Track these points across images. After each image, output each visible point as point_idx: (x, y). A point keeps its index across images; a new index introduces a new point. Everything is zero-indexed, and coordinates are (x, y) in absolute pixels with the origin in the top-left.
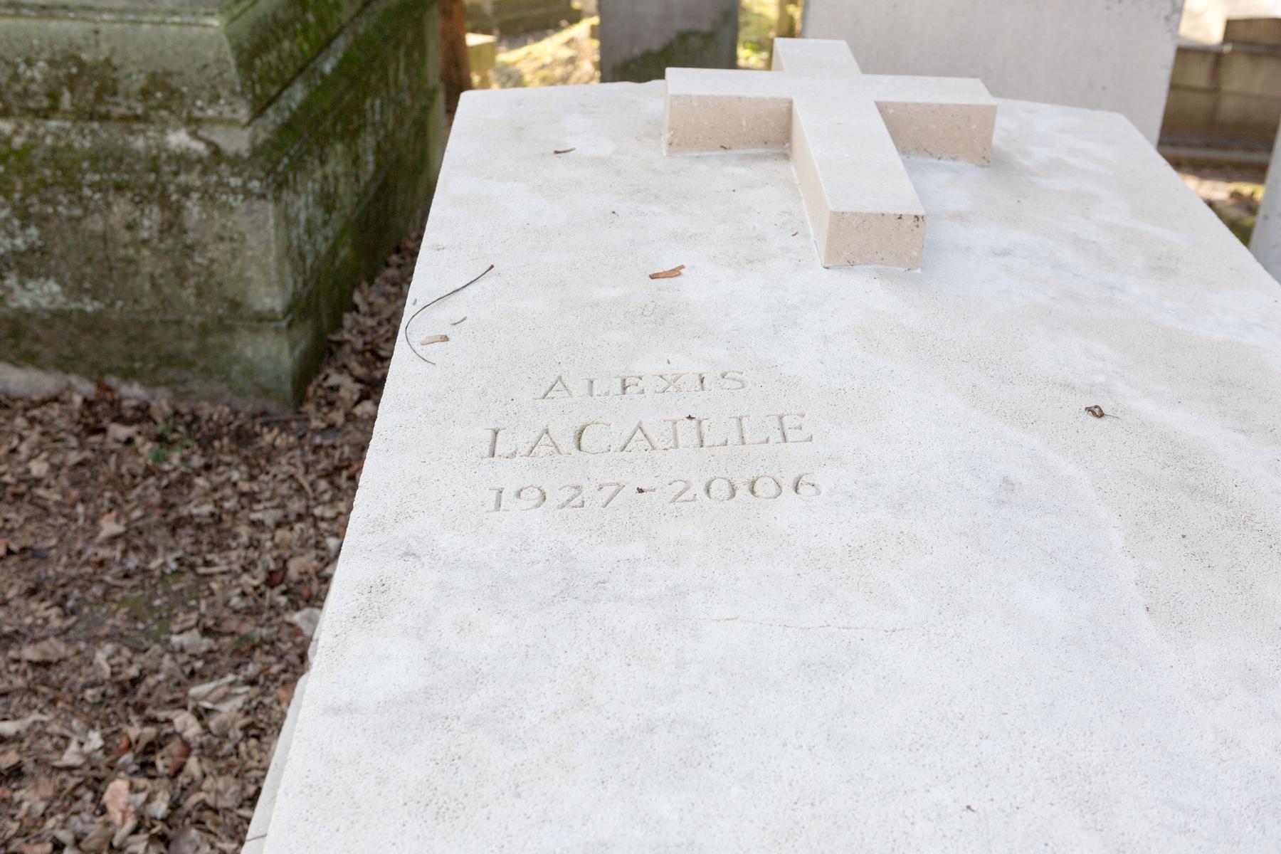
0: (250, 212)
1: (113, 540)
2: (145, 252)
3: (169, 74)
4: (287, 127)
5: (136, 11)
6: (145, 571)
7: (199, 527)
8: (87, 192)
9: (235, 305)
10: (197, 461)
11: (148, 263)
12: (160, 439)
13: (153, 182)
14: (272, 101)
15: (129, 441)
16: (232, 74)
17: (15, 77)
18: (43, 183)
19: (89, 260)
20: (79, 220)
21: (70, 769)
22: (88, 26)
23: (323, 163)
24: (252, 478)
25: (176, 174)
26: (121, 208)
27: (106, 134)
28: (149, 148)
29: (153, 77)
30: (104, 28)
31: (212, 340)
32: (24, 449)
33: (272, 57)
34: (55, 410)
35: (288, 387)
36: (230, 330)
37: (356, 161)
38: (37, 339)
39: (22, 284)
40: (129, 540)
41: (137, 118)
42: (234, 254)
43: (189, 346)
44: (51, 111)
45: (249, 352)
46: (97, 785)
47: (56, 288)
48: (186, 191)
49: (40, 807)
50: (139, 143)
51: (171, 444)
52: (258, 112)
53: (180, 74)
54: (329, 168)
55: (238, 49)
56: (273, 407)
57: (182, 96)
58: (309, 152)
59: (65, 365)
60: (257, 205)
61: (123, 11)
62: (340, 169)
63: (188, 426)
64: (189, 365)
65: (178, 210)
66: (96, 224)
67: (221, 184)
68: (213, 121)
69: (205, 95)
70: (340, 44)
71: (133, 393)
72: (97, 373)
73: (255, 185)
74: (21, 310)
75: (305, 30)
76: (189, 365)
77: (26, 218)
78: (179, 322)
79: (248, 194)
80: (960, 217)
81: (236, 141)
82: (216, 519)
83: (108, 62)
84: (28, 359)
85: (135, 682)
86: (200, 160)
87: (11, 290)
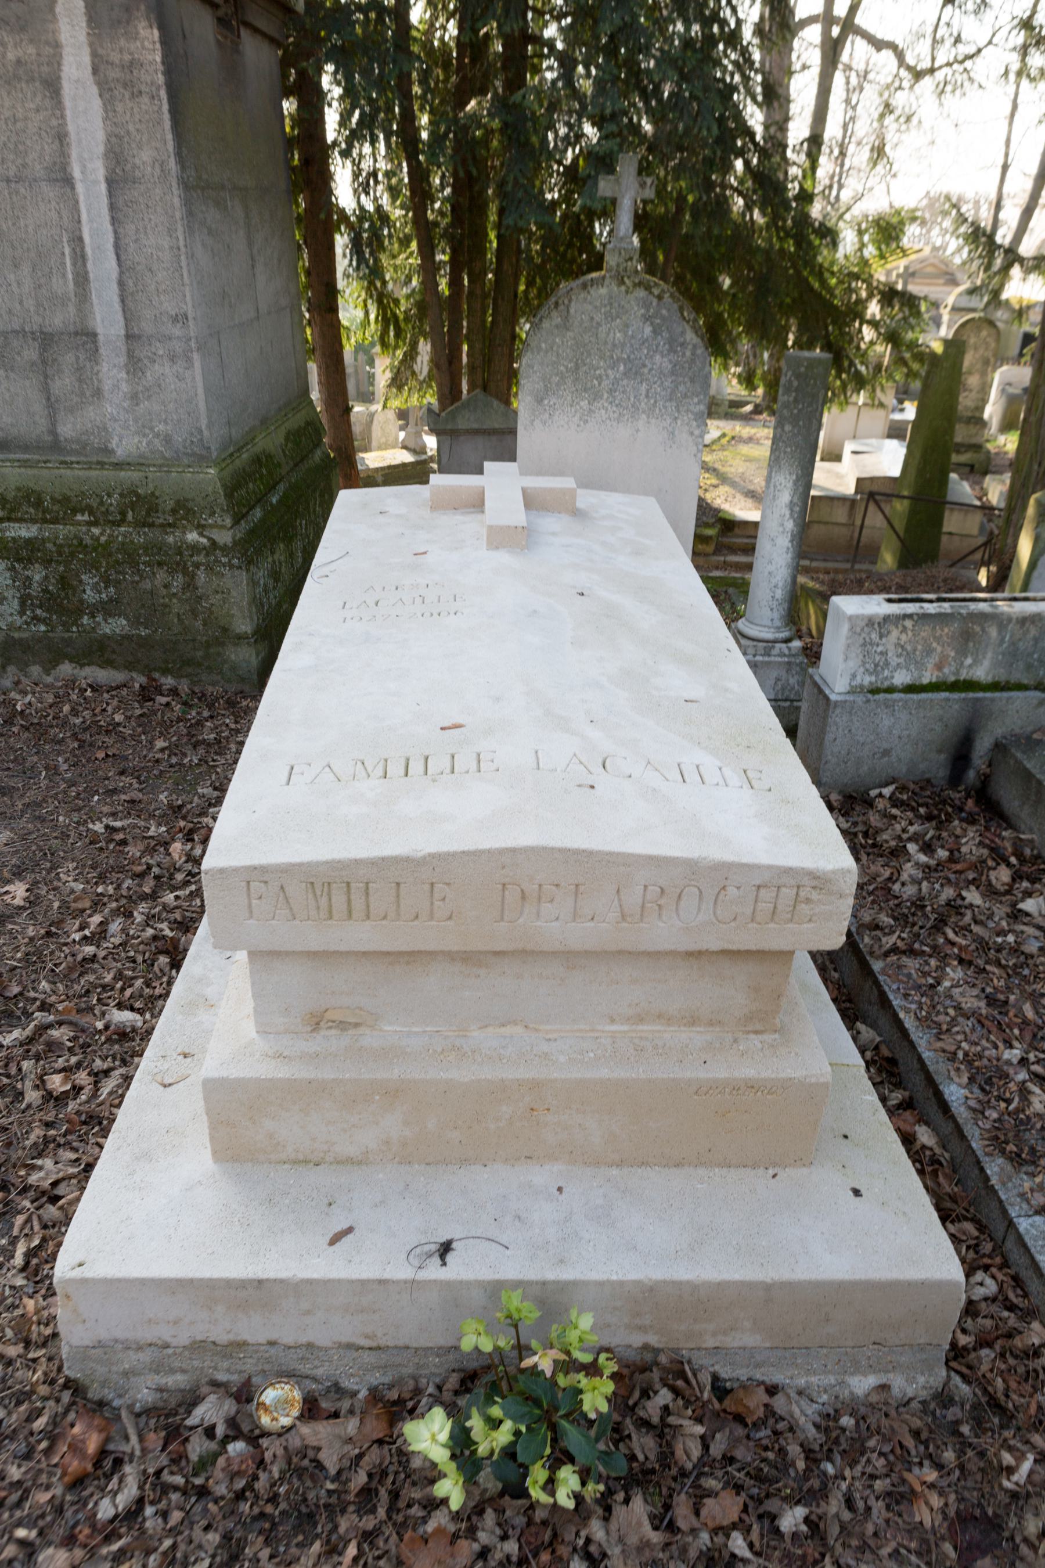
0: (233, 577)
1: (162, 750)
2: (175, 601)
3: (187, 500)
4: (252, 532)
5: (168, 466)
6: (181, 764)
7: (209, 745)
8: (142, 567)
9: (225, 630)
10: (206, 714)
11: (176, 607)
12: (185, 703)
13: (179, 560)
14: (244, 516)
15: (168, 704)
16: (222, 500)
17: (102, 503)
18: (117, 562)
19: (143, 605)
20: (137, 583)
21: (152, 837)
22: (141, 474)
23: (273, 553)
24: (236, 722)
25: (192, 556)
26: (161, 576)
27: (151, 534)
28: (176, 542)
29: (178, 502)
30: (150, 475)
31: (212, 650)
32: (109, 709)
33: (243, 492)
34: (124, 692)
35: (255, 677)
36: (223, 644)
37: (291, 555)
38: (114, 652)
39: (106, 620)
40: (171, 750)
41: (169, 525)
42: (224, 600)
43: (199, 654)
44: (123, 521)
45: (233, 657)
46: (166, 844)
47: (124, 622)
48: (197, 566)
49: (138, 854)
50: (171, 539)
51: (191, 707)
52: (236, 522)
53: (193, 500)
54: (276, 557)
55: (224, 486)
56: (247, 688)
57: (194, 512)
58: (265, 546)
59: (129, 666)
60: (237, 572)
61: (161, 466)
62: (282, 558)
63: (200, 699)
64: (199, 665)
65: (193, 576)
66: (147, 585)
67: (216, 561)
68: (211, 526)
69: (207, 511)
70: (281, 487)
71: (168, 681)
72: (147, 671)
73: (235, 561)
74: (105, 635)
75: (261, 478)
76: (199, 665)
77: (107, 582)
78: (194, 640)
79: (231, 566)
80: (554, 534)
81: (225, 537)
82: (218, 741)
83: (153, 493)
84: (108, 664)
85: (180, 807)
86: (205, 548)
87: (99, 624)
